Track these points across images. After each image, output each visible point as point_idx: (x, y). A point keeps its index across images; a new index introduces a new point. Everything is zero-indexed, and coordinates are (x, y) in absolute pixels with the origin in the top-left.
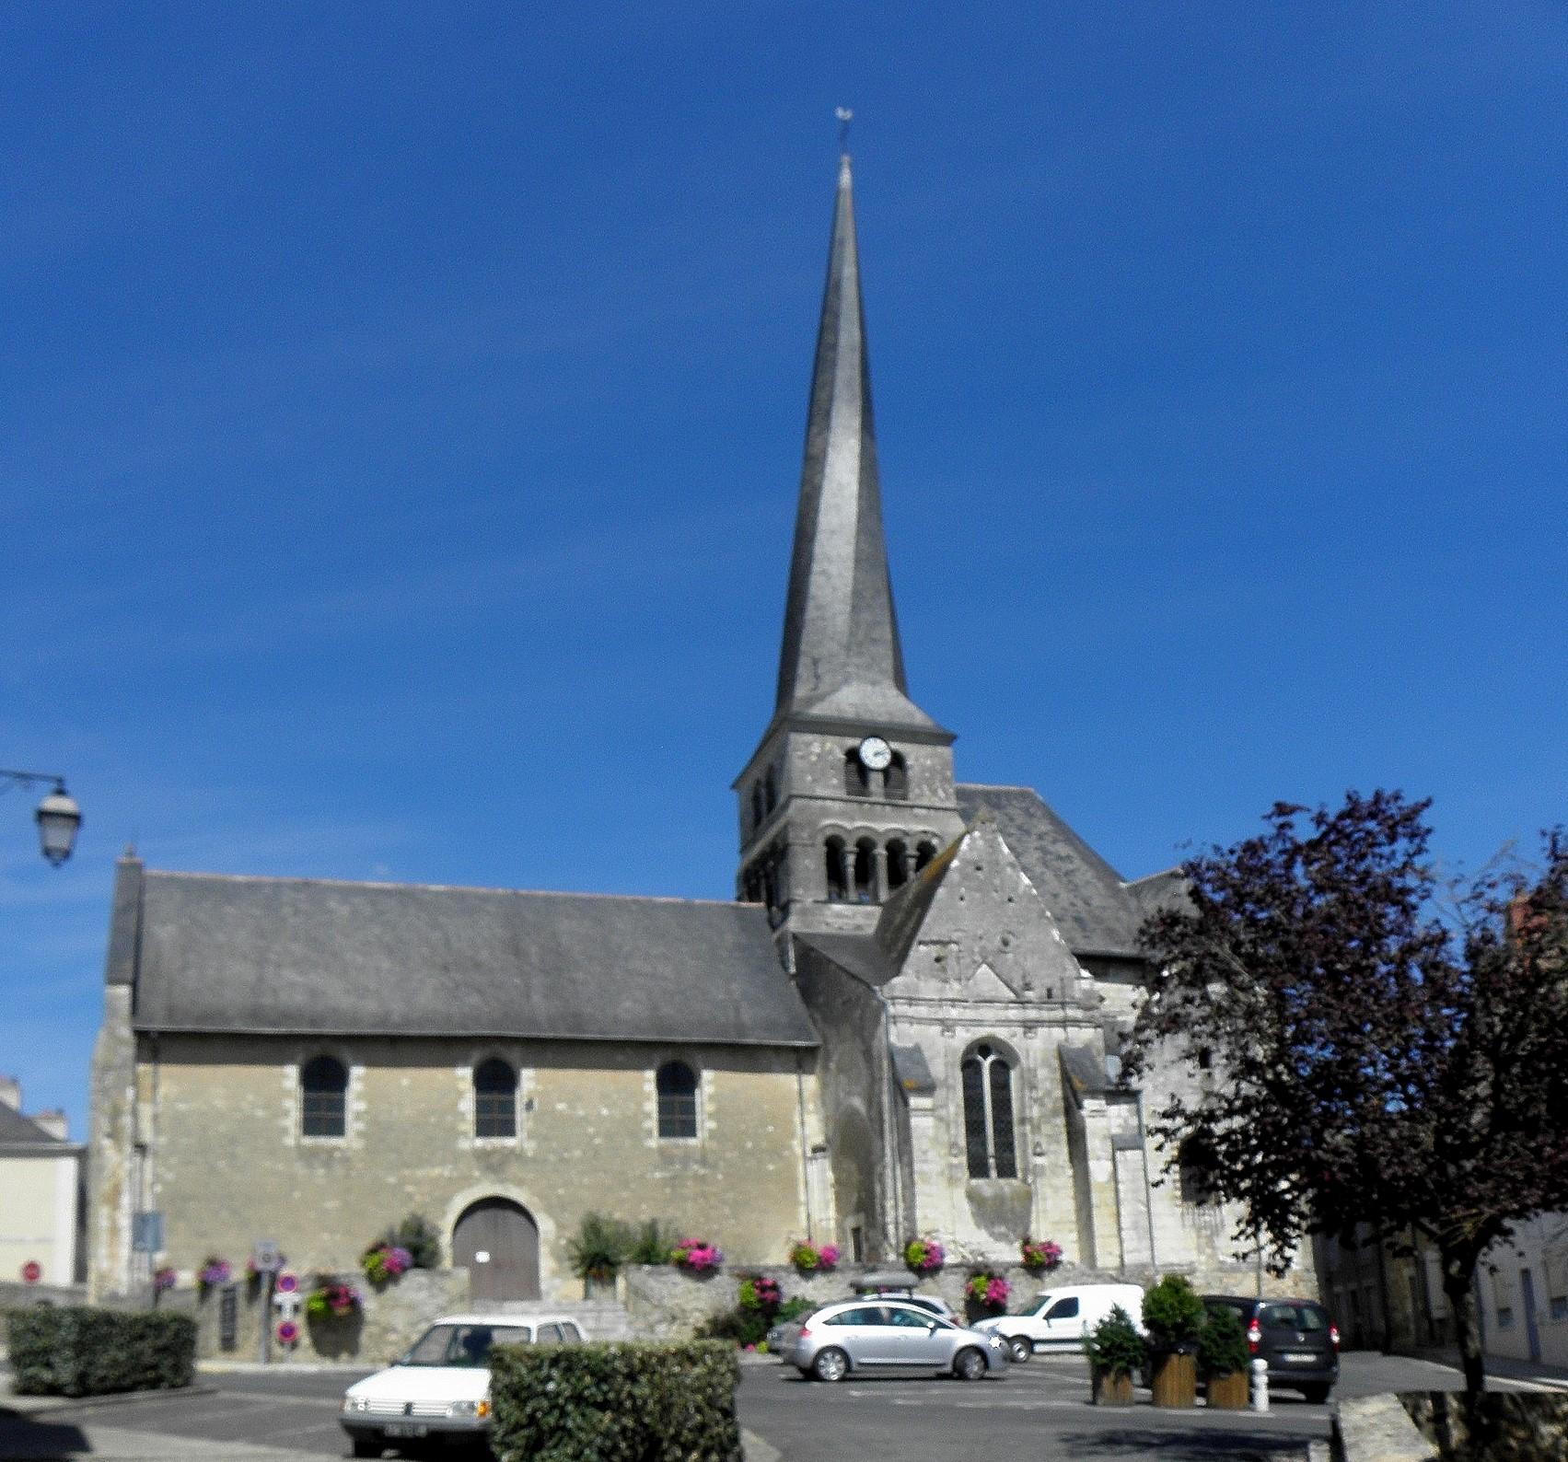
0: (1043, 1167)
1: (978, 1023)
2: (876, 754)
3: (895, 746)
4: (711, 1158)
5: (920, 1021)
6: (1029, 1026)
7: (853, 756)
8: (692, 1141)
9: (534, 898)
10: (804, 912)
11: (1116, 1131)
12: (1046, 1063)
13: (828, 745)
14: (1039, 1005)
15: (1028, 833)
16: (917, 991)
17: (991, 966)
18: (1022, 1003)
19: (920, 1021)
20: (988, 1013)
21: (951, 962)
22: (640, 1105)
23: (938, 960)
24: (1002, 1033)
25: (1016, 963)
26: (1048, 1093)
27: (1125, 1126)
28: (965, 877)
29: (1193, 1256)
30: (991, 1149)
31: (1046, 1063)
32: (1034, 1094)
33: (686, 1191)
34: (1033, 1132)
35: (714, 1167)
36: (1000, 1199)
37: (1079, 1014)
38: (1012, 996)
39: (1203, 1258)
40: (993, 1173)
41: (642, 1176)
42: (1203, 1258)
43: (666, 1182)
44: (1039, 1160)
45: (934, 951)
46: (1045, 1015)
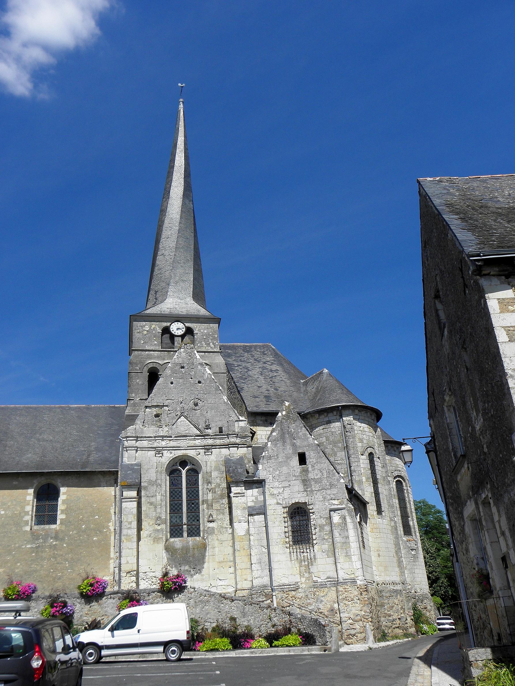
0: (213, 528)
1: (177, 448)
2: (178, 329)
3: (187, 325)
4: (61, 535)
5: (143, 449)
6: (208, 449)
7: (166, 331)
8: (53, 526)
9: (8, 408)
10: (134, 405)
11: (250, 504)
12: (217, 469)
13: (153, 326)
14: (214, 436)
15: (259, 361)
16: (142, 432)
17: (186, 417)
18: (204, 436)
19: (143, 449)
20: (183, 443)
21: (164, 417)
22: (23, 507)
23: (157, 416)
24: (191, 453)
25: (202, 415)
26: (219, 485)
27: (256, 501)
28: (174, 372)
29: (297, 579)
30: (185, 520)
31: (217, 469)
32: (209, 487)
33: (45, 555)
34: (208, 509)
35: (63, 540)
36: (186, 549)
37: (238, 441)
38: (198, 433)
39: (303, 580)
40: (185, 534)
41: (19, 547)
42: (303, 580)
43: (32, 550)
44: (211, 525)
45: (155, 411)
46: (218, 442)
